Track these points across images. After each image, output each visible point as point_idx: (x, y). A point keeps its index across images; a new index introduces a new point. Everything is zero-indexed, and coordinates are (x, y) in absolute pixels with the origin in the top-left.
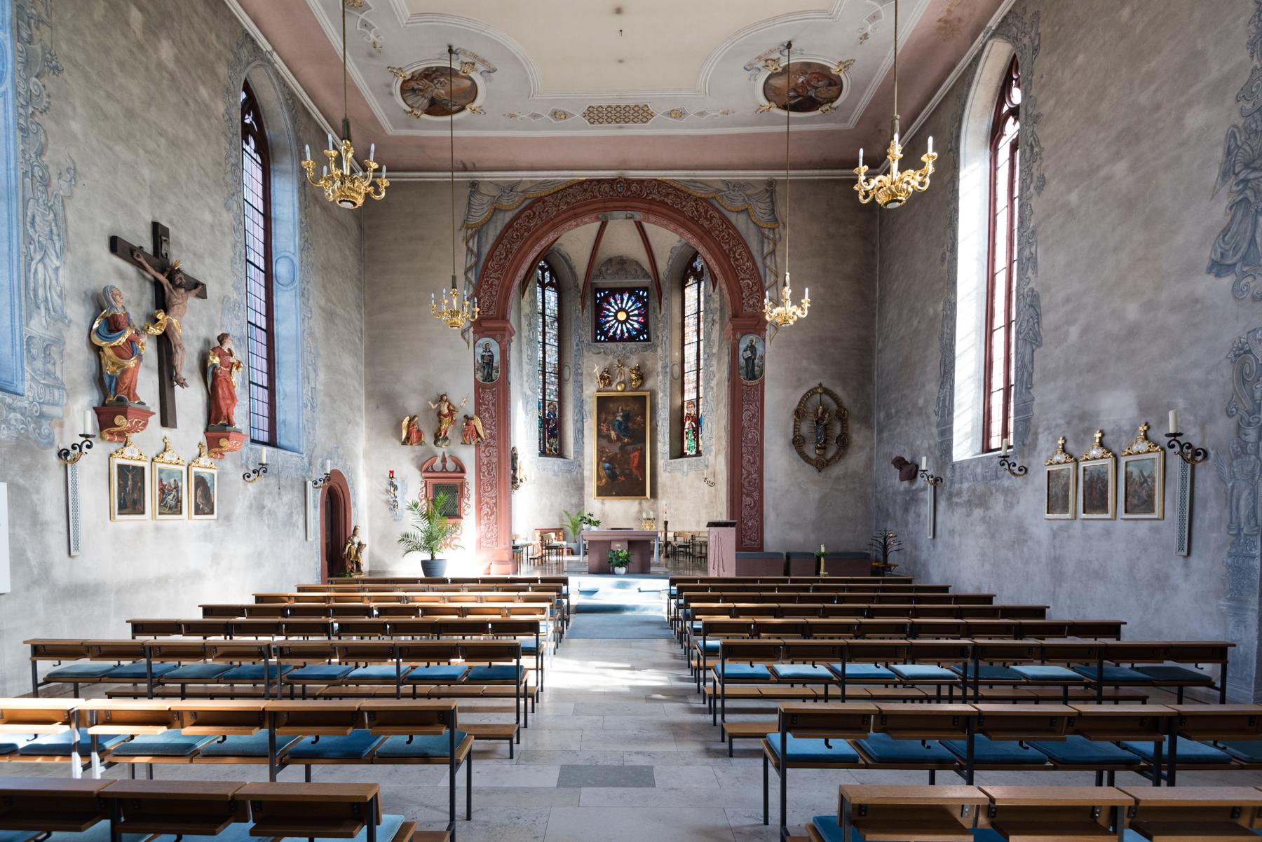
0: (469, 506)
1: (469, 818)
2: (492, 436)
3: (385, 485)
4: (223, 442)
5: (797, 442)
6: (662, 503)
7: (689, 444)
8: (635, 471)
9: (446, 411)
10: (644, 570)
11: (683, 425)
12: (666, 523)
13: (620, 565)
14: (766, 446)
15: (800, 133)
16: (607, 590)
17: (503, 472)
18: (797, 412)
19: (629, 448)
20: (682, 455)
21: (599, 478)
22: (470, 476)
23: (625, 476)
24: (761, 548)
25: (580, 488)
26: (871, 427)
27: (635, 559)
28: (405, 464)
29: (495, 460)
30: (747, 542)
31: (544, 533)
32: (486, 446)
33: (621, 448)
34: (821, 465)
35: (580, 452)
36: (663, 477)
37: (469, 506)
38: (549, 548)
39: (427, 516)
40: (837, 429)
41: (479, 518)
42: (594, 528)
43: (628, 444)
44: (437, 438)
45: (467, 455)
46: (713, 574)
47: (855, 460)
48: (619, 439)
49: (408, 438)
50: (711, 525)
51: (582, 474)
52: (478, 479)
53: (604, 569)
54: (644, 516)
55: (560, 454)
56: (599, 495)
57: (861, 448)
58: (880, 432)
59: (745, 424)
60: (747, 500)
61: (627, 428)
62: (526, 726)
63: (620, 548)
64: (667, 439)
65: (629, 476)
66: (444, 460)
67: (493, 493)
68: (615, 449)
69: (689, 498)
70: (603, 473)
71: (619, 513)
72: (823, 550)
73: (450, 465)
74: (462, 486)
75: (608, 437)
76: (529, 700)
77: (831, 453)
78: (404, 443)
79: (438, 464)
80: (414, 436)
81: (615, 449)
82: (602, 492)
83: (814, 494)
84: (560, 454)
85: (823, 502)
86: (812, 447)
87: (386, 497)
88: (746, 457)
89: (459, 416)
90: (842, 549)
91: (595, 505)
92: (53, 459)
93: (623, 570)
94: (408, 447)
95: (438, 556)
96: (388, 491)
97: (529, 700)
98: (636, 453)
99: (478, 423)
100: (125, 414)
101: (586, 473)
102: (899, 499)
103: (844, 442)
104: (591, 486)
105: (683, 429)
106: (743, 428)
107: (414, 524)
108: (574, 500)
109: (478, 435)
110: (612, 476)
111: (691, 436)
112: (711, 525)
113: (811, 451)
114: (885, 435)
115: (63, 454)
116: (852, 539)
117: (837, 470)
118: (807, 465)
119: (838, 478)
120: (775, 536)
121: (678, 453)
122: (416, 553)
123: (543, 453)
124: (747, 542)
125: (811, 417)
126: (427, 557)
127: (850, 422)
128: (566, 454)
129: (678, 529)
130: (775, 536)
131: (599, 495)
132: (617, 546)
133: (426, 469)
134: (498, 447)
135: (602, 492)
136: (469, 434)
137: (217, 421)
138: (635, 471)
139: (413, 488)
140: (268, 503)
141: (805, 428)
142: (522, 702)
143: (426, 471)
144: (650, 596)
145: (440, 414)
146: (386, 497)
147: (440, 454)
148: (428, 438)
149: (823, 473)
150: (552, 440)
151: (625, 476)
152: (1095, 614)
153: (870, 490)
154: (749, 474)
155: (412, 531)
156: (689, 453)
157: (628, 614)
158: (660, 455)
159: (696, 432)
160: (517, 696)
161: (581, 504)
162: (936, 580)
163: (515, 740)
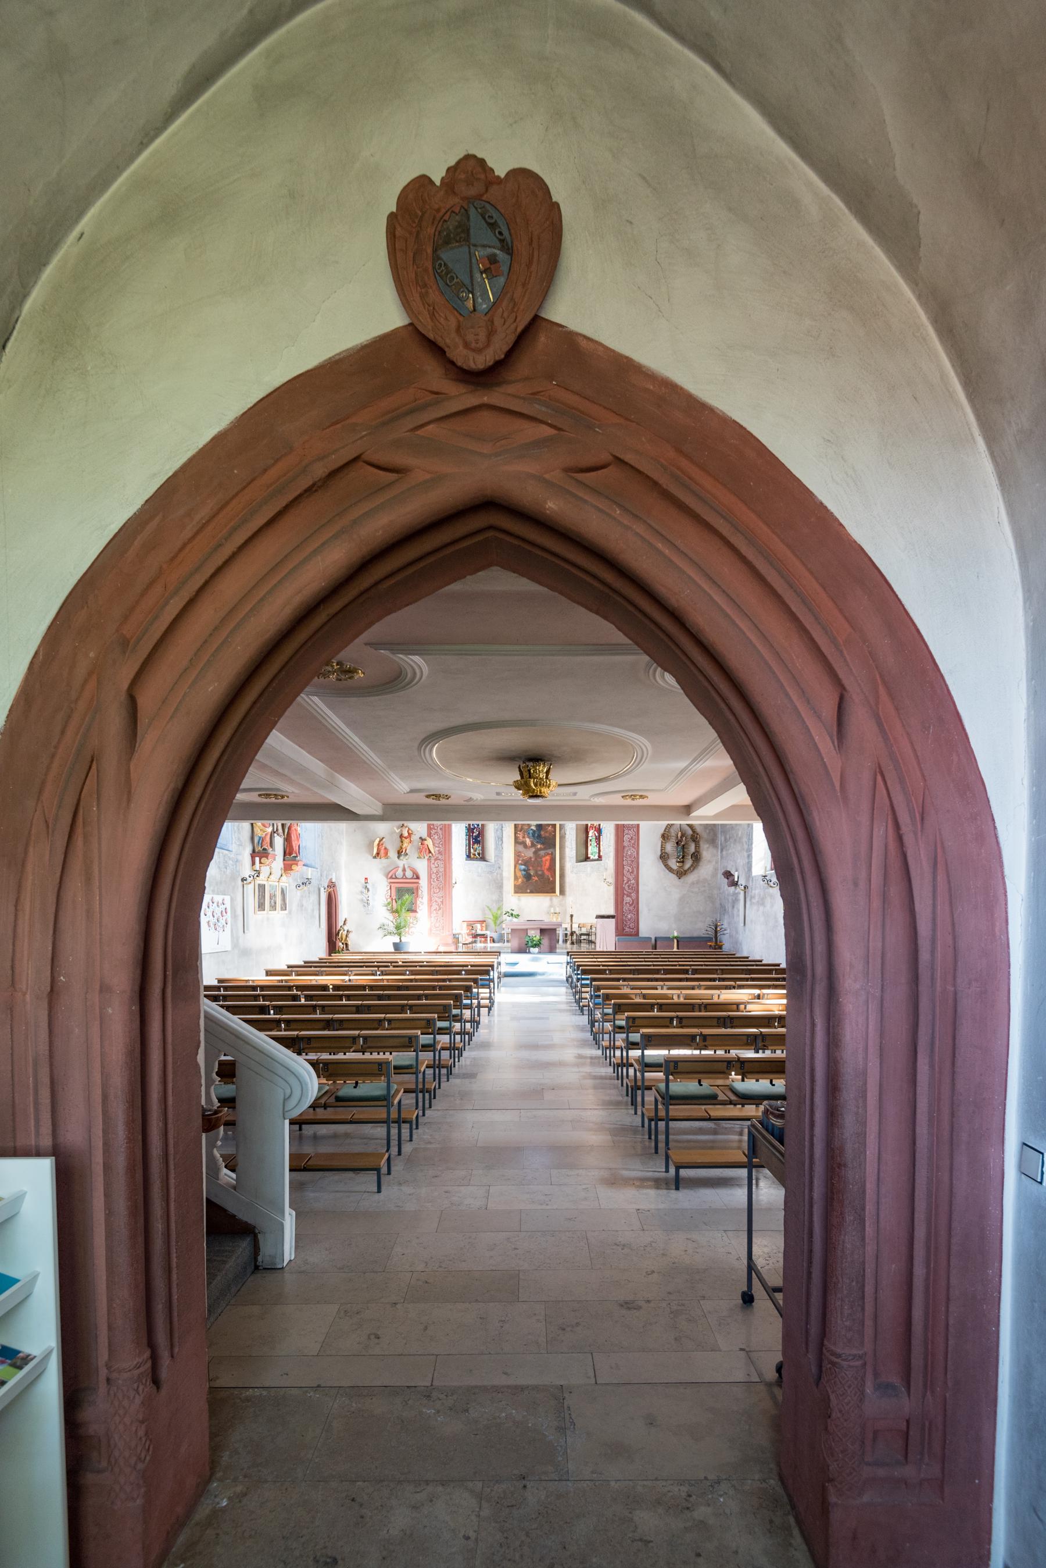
0: (422, 903)
1: (389, 1173)
2: (440, 853)
3: (360, 888)
4: (294, 867)
5: (664, 857)
6: (570, 898)
7: (592, 850)
8: (547, 873)
9: (406, 834)
10: (552, 950)
11: (587, 833)
12: (572, 916)
13: (535, 946)
14: (641, 860)
15: (515, 1005)
16: (524, 962)
17: (443, 880)
18: (663, 836)
19: (542, 853)
20: (587, 858)
21: (516, 878)
22: (423, 882)
23: (539, 877)
24: (637, 934)
25: (500, 887)
26: (716, 847)
27: (545, 942)
28: (376, 872)
29: (442, 870)
30: (627, 929)
31: (471, 925)
32: (436, 860)
33: (535, 853)
34: (681, 874)
35: (499, 856)
36: (570, 877)
37: (422, 903)
38: (476, 936)
39: (394, 911)
40: (692, 848)
41: (430, 912)
42: (515, 920)
43: (541, 849)
44: (399, 853)
45: (422, 866)
46: (598, 949)
47: (705, 870)
48: (533, 845)
49: (378, 854)
50: (598, 917)
51: (501, 875)
52: (430, 883)
53: (523, 950)
54: (552, 911)
55: (482, 858)
56: (516, 892)
57: (709, 861)
58: (722, 850)
59: (626, 844)
60: (627, 899)
61: (539, 836)
62: (400, 1153)
63: (535, 935)
64: (574, 846)
65: (541, 876)
66: (404, 870)
67: (441, 894)
68: (529, 853)
69: (586, 896)
70: (519, 874)
71: (535, 908)
72: (676, 934)
73: (409, 874)
74: (417, 889)
75: (524, 844)
76: (427, 1095)
77: (687, 865)
78: (375, 857)
79: (400, 873)
80: (382, 852)
81: (529, 853)
82: (519, 890)
83: (676, 894)
84: (482, 858)
85: (682, 900)
86: (674, 861)
87: (360, 897)
88: (626, 868)
89: (415, 838)
90: (695, 935)
91: (513, 901)
92: (240, 883)
93: (536, 950)
94: (378, 860)
95: (404, 939)
96: (362, 892)
97: (427, 1095)
98: (548, 857)
99: (429, 842)
100: (267, 857)
101: (505, 874)
102: (730, 898)
103: (697, 857)
104: (509, 884)
105: (587, 837)
106: (624, 847)
107: (382, 915)
108: (495, 897)
109: (430, 852)
110: (528, 877)
111: (594, 843)
112: (598, 917)
113: (673, 864)
114: (724, 853)
115: (243, 880)
116: (700, 928)
117: (692, 878)
118: (671, 874)
119: (693, 883)
120: (649, 925)
121: (584, 857)
122: (389, 937)
123: (469, 857)
124: (627, 929)
125: (673, 840)
126: (396, 939)
127: (701, 843)
128: (487, 857)
129: (582, 921)
130: (649, 925)
131: (516, 892)
132: (531, 933)
133: (391, 876)
134: (445, 861)
135: (519, 890)
136: (423, 849)
137: (290, 854)
138: (547, 873)
139: (381, 891)
140: (304, 903)
141: (670, 847)
142: (394, 1131)
143: (391, 878)
144: (555, 965)
145: (401, 836)
146: (360, 897)
147: (401, 866)
148: (392, 854)
149: (682, 880)
150: (476, 846)
151: (539, 877)
152: (758, 958)
153: (715, 892)
154: (629, 880)
155: (386, 922)
156: (592, 857)
157: (539, 977)
158: (567, 859)
159: (598, 839)
160: (386, 1122)
161: (500, 900)
162: (745, 955)
163: (414, 1127)
